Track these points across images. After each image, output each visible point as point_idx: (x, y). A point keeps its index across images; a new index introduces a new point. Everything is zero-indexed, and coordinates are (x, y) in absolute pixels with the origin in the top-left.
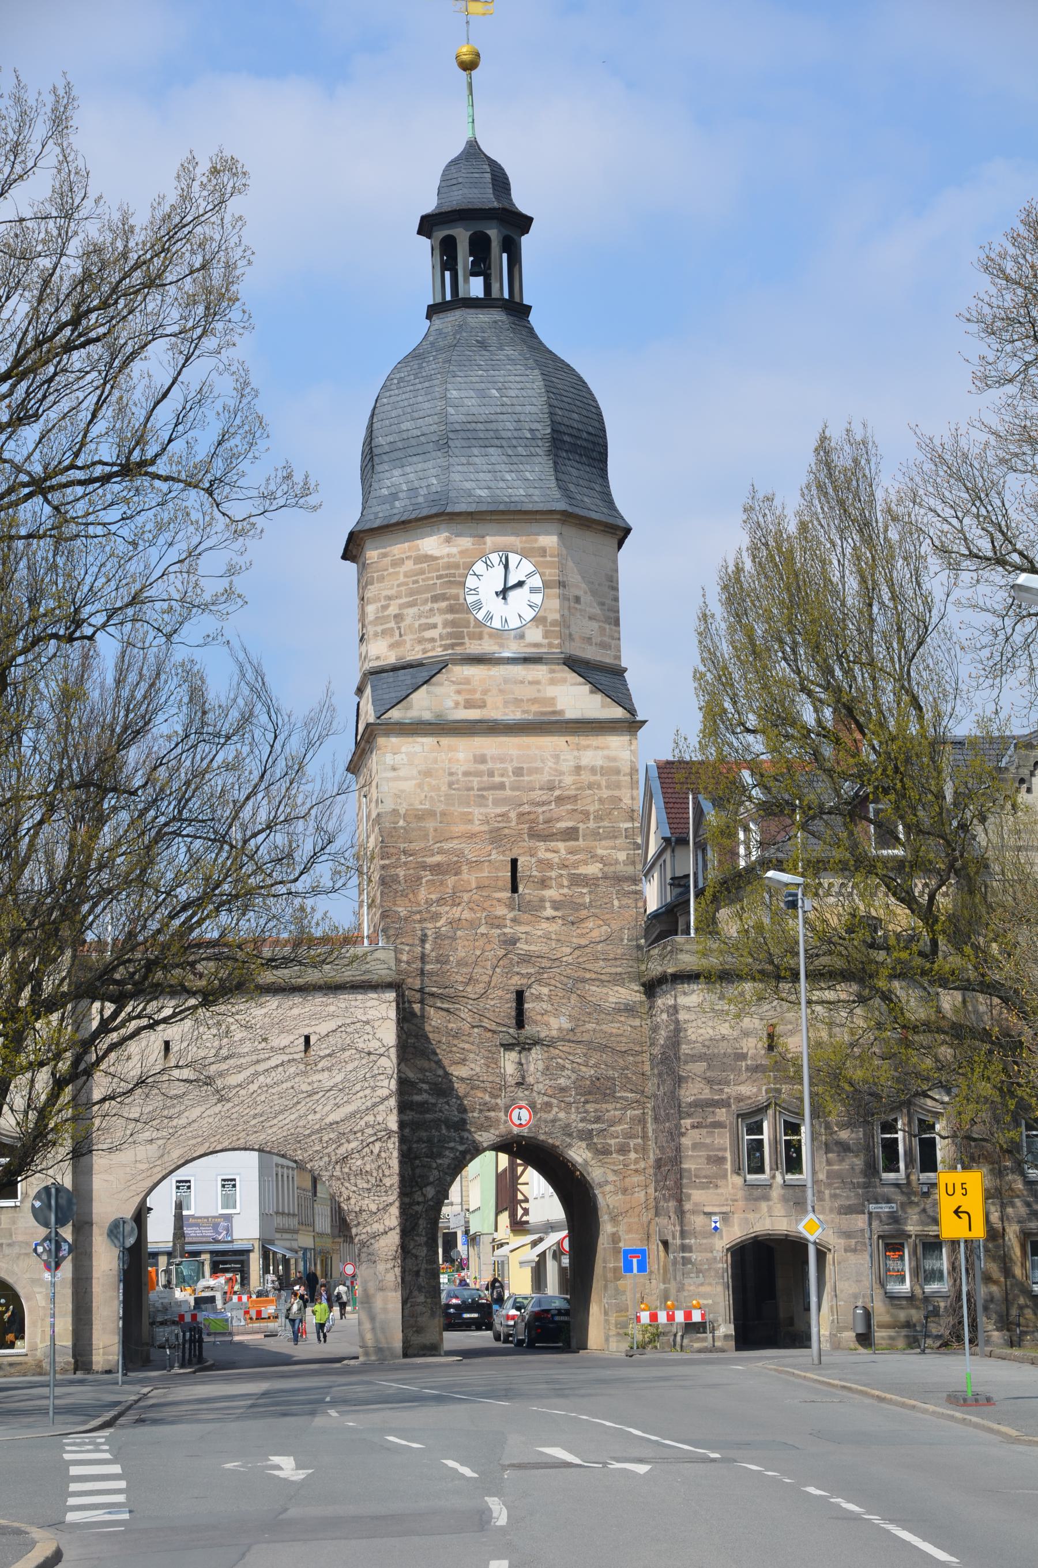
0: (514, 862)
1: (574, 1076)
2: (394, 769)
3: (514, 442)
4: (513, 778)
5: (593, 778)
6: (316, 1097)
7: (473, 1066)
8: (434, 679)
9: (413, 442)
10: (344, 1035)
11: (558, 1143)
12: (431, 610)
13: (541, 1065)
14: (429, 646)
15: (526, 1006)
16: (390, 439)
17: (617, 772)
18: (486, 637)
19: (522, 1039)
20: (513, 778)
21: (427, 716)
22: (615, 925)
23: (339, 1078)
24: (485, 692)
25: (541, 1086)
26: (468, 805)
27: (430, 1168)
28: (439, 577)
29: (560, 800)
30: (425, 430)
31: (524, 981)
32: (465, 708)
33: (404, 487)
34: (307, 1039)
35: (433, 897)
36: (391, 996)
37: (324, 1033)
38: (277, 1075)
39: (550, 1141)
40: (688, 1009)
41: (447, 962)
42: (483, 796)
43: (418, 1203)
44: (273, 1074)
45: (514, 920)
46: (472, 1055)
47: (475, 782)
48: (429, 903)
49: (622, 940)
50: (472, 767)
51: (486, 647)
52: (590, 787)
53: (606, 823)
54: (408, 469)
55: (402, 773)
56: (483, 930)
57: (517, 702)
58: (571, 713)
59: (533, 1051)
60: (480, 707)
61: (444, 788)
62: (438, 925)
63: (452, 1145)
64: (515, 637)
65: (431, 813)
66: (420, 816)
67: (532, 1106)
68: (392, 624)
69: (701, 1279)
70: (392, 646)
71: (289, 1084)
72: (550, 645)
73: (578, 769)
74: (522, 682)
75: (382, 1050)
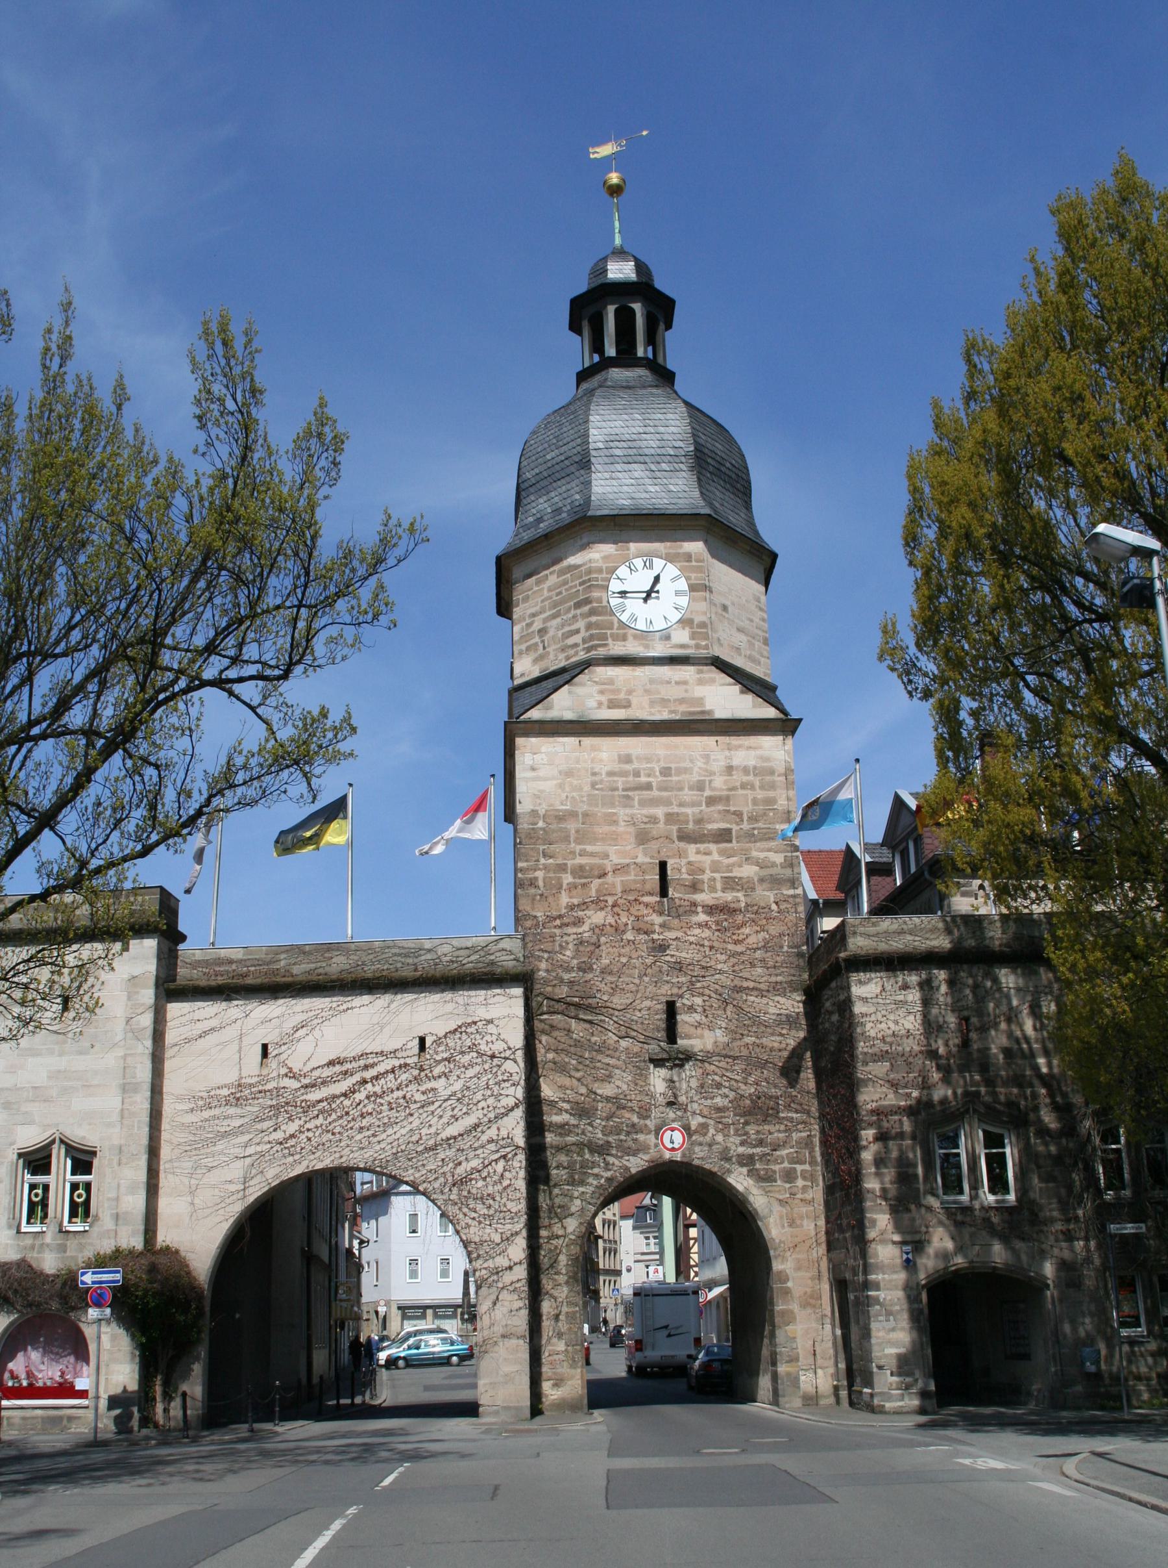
0: (663, 866)
1: (732, 1095)
2: (533, 769)
3: (658, 459)
4: (660, 778)
5: (745, 779)
6: (432, 1108)
7: (618, 1083)
8: (576, 680)
9: (557, 468)
10: (464, 1036)
11: (715, 1169)
12: (574, 617)
13: (694, 1083)
14: (572, 652)
15: (679, 1017)
16: (533, 473)
17: (772, 772)
18: (630, 638)
19: (674, 1055)
20: (660, 778)
21: (569, 716)
22: (775, 929)
23: (458, 1086)
24: (630, 692)
25: (695, 1106)
26: (613, 805)
27: (572, 1198)
28: (581, 584)
29: (711, 801)
30: (569, 454)
31: (675, 991)
32: (609, 708)
33: (549, 510)
34: (422, 1040)
35: (576, 901)
36: (518, 991)
37: (441, 1034)
38: (390, 1082)
39: (707, 1166)
40: (865, 1000)
41: (591, 969)
42: (628, 797)
43: (558, 1237)
44: (382, 1081)
45: (663, 926)
46: (617, 1071)
47: (620, 782)
48: (572, 908)
49: (781, 947)
50: (617, 767)
51: (631, 648)
52: (743, 786)
53: (760, 825)
54: (553, 494)
55: (541, 773)
56: (629, 936)
57: (664, 702)
58: (721, 713)
59: (687, 1067)
60: (625, 707)
61: (587, 788)
62: (580, 930)
63: (596, 1171)
64: (661, 639)
65: (573, 814)
66: (561, 818)
67: (687, 1128)
68: (537, 639)
69: (892, 1323)
70: (535, 661)
71: (400, 1094)
72: (697, 646)
73: (730, 769)
74: (669, 682)
75: (508, 1053)
